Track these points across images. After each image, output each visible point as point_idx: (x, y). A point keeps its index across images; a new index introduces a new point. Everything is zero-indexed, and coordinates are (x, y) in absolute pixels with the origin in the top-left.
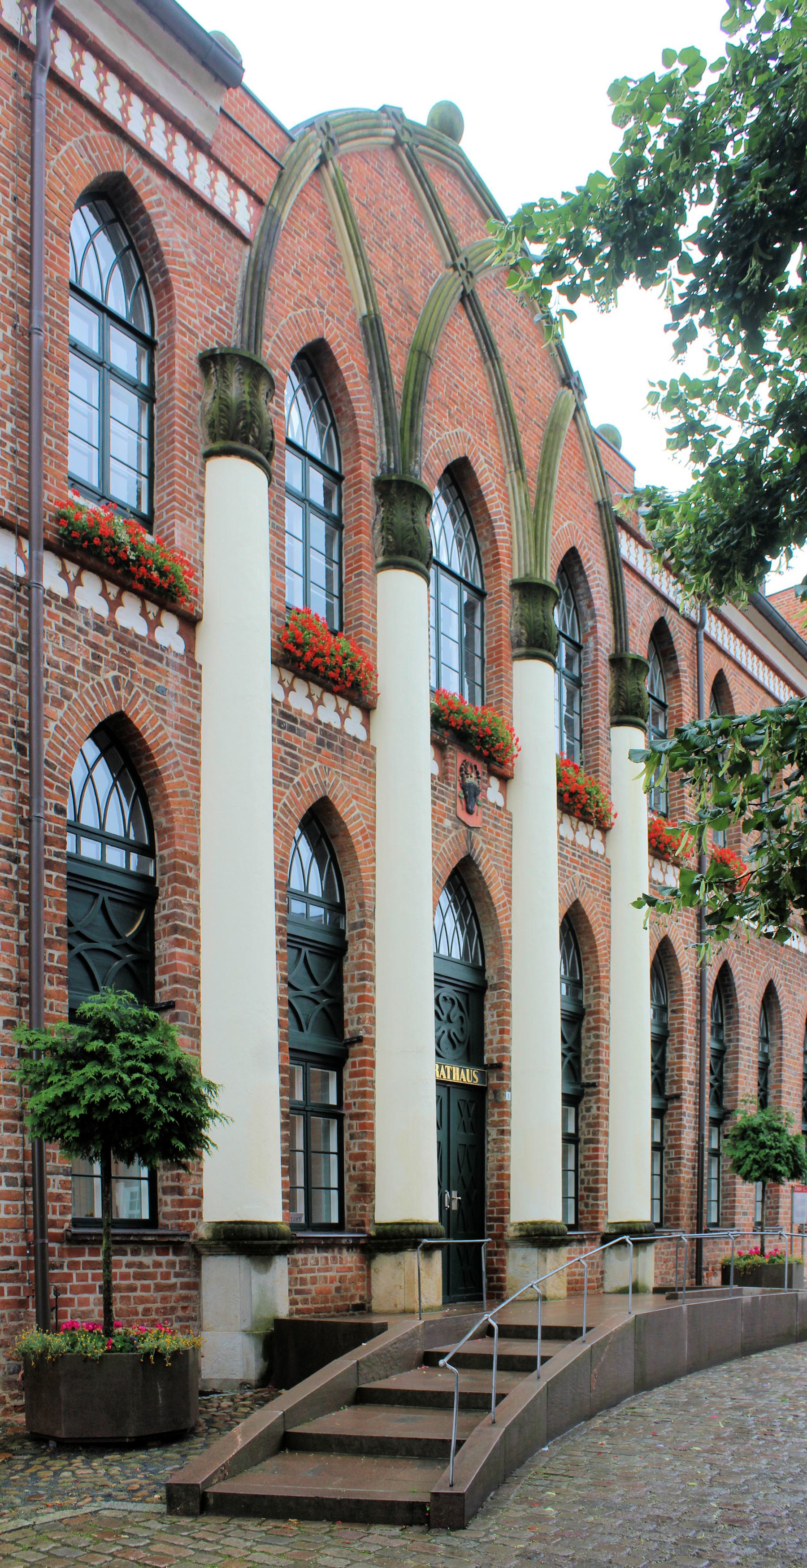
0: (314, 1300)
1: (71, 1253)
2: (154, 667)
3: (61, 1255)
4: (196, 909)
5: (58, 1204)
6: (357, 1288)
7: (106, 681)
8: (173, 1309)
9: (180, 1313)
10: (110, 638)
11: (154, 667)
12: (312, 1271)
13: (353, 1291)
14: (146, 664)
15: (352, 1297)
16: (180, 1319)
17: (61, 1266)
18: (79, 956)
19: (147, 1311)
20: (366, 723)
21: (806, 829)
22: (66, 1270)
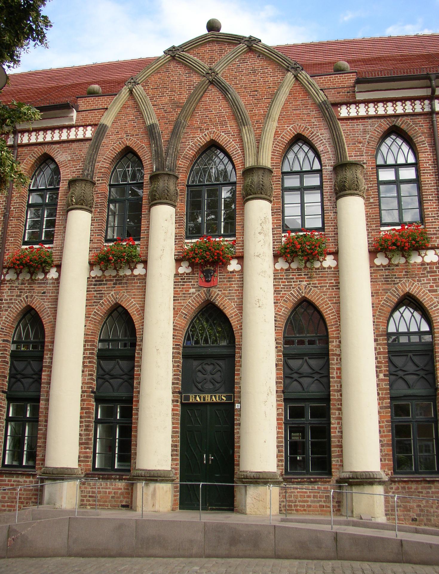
6: (125, 498)
7: (23, 298)
10: (27, 285)
12: (99, 488)
14: (39, 287)
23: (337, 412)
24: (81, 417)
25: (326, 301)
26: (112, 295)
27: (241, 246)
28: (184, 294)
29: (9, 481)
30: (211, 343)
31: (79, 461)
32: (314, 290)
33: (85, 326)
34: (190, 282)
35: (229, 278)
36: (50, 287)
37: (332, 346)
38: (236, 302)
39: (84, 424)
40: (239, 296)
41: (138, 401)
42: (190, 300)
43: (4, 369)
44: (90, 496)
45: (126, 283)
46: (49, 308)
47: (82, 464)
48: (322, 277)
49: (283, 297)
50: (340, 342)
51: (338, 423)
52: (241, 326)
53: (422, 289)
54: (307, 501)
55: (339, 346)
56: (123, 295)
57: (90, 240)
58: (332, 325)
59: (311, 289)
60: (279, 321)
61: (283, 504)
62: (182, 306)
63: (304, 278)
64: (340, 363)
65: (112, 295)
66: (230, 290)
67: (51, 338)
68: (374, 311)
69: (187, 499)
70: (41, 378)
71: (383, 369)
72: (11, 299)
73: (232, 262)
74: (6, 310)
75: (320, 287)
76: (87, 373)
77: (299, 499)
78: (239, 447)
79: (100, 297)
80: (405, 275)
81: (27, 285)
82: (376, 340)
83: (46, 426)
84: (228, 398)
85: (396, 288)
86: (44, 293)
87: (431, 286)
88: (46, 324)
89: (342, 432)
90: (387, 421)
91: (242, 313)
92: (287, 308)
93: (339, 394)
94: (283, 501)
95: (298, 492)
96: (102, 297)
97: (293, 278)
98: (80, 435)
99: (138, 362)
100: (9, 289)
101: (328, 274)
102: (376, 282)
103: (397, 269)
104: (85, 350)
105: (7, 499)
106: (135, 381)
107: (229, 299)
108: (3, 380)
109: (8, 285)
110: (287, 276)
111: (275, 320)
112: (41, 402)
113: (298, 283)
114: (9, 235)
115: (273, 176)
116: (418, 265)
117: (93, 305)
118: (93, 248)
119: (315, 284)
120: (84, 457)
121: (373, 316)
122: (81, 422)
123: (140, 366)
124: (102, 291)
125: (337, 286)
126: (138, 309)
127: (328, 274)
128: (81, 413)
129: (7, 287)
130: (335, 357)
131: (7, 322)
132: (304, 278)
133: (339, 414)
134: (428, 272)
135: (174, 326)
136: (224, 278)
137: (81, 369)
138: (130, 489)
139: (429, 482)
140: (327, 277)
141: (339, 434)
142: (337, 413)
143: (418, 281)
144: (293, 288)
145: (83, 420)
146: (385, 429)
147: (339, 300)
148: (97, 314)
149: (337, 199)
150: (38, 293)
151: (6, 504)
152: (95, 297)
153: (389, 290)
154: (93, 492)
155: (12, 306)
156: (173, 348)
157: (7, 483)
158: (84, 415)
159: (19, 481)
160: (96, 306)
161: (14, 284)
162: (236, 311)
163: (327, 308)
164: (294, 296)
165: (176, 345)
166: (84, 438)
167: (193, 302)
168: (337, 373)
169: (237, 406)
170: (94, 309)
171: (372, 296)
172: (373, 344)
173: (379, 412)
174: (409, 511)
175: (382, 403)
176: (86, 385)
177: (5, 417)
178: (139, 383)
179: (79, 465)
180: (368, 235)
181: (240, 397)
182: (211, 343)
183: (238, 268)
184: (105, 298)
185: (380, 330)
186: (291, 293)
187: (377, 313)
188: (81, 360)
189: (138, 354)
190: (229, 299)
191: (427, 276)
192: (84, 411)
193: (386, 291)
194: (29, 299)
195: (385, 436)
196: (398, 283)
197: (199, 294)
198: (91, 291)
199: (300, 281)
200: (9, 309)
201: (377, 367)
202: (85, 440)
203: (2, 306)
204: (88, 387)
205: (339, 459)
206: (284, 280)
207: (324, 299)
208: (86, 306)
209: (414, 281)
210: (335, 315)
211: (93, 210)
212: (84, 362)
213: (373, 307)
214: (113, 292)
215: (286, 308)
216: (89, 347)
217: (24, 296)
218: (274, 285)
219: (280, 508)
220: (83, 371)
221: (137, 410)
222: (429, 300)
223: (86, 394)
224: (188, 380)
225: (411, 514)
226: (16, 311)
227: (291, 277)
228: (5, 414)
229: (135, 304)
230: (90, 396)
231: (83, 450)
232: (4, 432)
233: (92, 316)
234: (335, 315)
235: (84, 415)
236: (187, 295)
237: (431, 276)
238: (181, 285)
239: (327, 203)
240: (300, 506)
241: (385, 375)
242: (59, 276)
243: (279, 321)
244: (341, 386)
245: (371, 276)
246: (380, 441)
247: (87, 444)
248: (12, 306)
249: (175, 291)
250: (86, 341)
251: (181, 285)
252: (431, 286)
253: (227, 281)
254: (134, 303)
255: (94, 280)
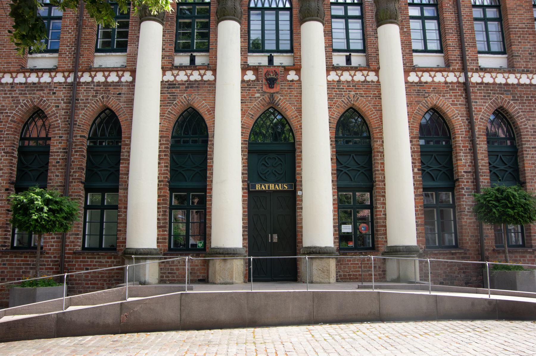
0: (177, 277)
1: (76, 258)
2: (117, 89)
3: (73, 258)
4: (129, 152)
5: (72, 244)
6: (201, 273)
7: (99, 98)
8: (113, 277)
9: (115, 278)
10: (102, 87)
11: (117, 89)
12: (177, 266)
13: (199, 274)
14: (114, 89)
15: (198, 276)
16: (115, 280)
17: (73, 262)
18: (494, 173)
19: (102, 277)
20: (377, 75)
21: (380, 1)
22: (74, 263)
23: (382, 199)
24: (158, 204)
25: (371, 108)
26: (185, 97)
27: (299, 60)
28: (250, 98)
29: (91, 262)
30: (273, 148)
31: (158, 242)
32: (361, 99)
33: (160, 124)
34: (255, 88)
35: (290, 86)
36: (124, 90)
37: (377, 144)
38: (296, 106)
39: (161, 210)
40: (298, 101)
41: (211, 189)
42: (255, 103)
43: (82, 162)
44: (169, 273)
45: (197, 87)
46: (124, 107)
47: (161, 245)
48: (367, 89)
49: (336, 103)
50: (383, 142)
51: (383, 208)
52: (301, 126)
53: (445, 103)
54: (359, 271)
55: (382, 145)
56: (195, 98)
57: (163, 49)
58: (376, 128)
59: (358, 98)
60: (332, 123)
61: (339, 274)
62: (249, 108)
63: (352, 89)
64: (383, 159)
65: (185, 97)
66: (290, 96)
67: (128, 134)
68: (409, 118)
69: (258, 273)
70: (119, 170)
71: (417, 164)
72: (87, 99)
73: (290, 72)
74: (83, 109)
75: (366, 96)
76: (163, 165)
77: (352, 269)
78: (302, 227)
79: (173, 98)
80: (432, 91)
81: (102, 87)
82: (411, 141)
83: (126, 212)
84: (290, 186)
85: (426, 101)
86: (120, 94)
87: (453, 101)
88: (123, 121)
89: (385, 215)
90: (420, 206)
91: (301, 115)
92: (338, 113)
93: (383, 183)
94: (339, 272)
95: (351, 264)
96: (175, 98)
97: (343, 89)
98: (158, 219)
99: (211, 155)
100: (85, 91)
101: (372, 86)
102: (410, 95)
103: (426, 86)
104: (160, 144)
105: (90, 278)
106: (208, 172)
107: (290, 103)
108: (82, 172)
109: (83, 86)
110: (338, 86)
111: (330, 122)
112: (120, 191)
113: (348, 92)
114: (83, 42)
115: (324, 4)
116: (443, 84)
117: (167, 106)
118: (166, 56)
119: (362, 94)
120: (163, 239)
121: (409, 122)
122: (158, 208)
123: (212, 159)
124: (175, 93)
125: (379, 97)
126: (209, 109)
127: (372, 86)
128: (158, 200)
129: (82, 88)
130: (379, 154)
131: (84, 119)
132: (352, 89)
133: (383, 200)
134: (450, 90)
135: (242, 125)
136: (285, 86)
137: (157, 161)
138: (206, 265)
139: (453, 254)
140: (371, 89)
141: (384, 216)
142: (382, 199)
143: (444, 96)
144: (344, 96)
145: (161, 206)
146: (419, 212)
147: (381, 108)
148: (171, 113)
149: (378, 26)
150: (114, 94)
151: (89, 282)
152: (168, 98)
153: (420, 102)
154: (172, 269)
155: (89, 105)
156: (242, 144)
157: (89, 263)
158: (162, 201)
159: (101, 262)
160: (170, 106)
161: (91, 85)
162: (296, 114)
163: (372, 114)
164: (344, 103)
165: (244, 141)
166: (161, 222)
167: (259, 104)
168: (381, 167)
169: (299, 193)
170: (168, 108)
171: (408, 106)
172: (409, 145)
173: (415, 199)
174: (438, 277)
175: (417, 192)
176: (162, 176)
177: (83, 206)
178: (212, 174)
179: (158, 246)
180: (403, 57)
181: (301, 186)
182: (273, 148)
183: (296, 78)
184: (178, 100)
185: (415, 133)
186: (342, 101)
187: (412, 120)
188: (157, 154)
189: (210, 148)
190: (290, 103)
191: (450, 93)
192: (162, 198)
193: (418, 102)
194: (105, 99)
195: (420, 218)
196: (427, 97)
197: (263, 99)
198: (165, 93)
199: (349, 91)
200: (85, 108)
201: (413, 163)
202: (163, 223)
203: (79, 105)
204: (164, 178)
205: (384, 237)
206: (336, 90)
207: (369, 106)
208: (161, 106)
209: (440, 96)
210: (378, 120)
211: (165, 23)
212: (159, 156)
213: (408, 115)
214: (185, 95)
215: (338, 112)
216: (164, 142)
217: (100, 97)
218: (328, 93)
219: (337, 277)
220: (159, 163)
221: (211, 196)
222: (451, 111)
223: (162, 183)
224: (253, 172)
225: (439, 279)
226: (92, 110)
227: (341, 87)
228: (83, 203)
229: (206, 105)
230: (166, 185)
231: (161, 233)
232: (83, 219)
233: (166, 115)
234: (378, 120)
235: (162, 201)
236: (252, 99)
237: (452, 93)
238: (247, 90)
239: (369, 30)
240: (354, 275)
241: (418, 170)
242: (134, 79)
243: (332, 123)
244: (384, 177)
245: (406, 90)
246: (416, 222)
247: (165, 227)
248: (89, 105)
249: (242, 95)
250: (161, 137)
251: (247, 90)
252: (453, 101)
253: (288, 89)
254: (205, 104)
255: (167, 84)
